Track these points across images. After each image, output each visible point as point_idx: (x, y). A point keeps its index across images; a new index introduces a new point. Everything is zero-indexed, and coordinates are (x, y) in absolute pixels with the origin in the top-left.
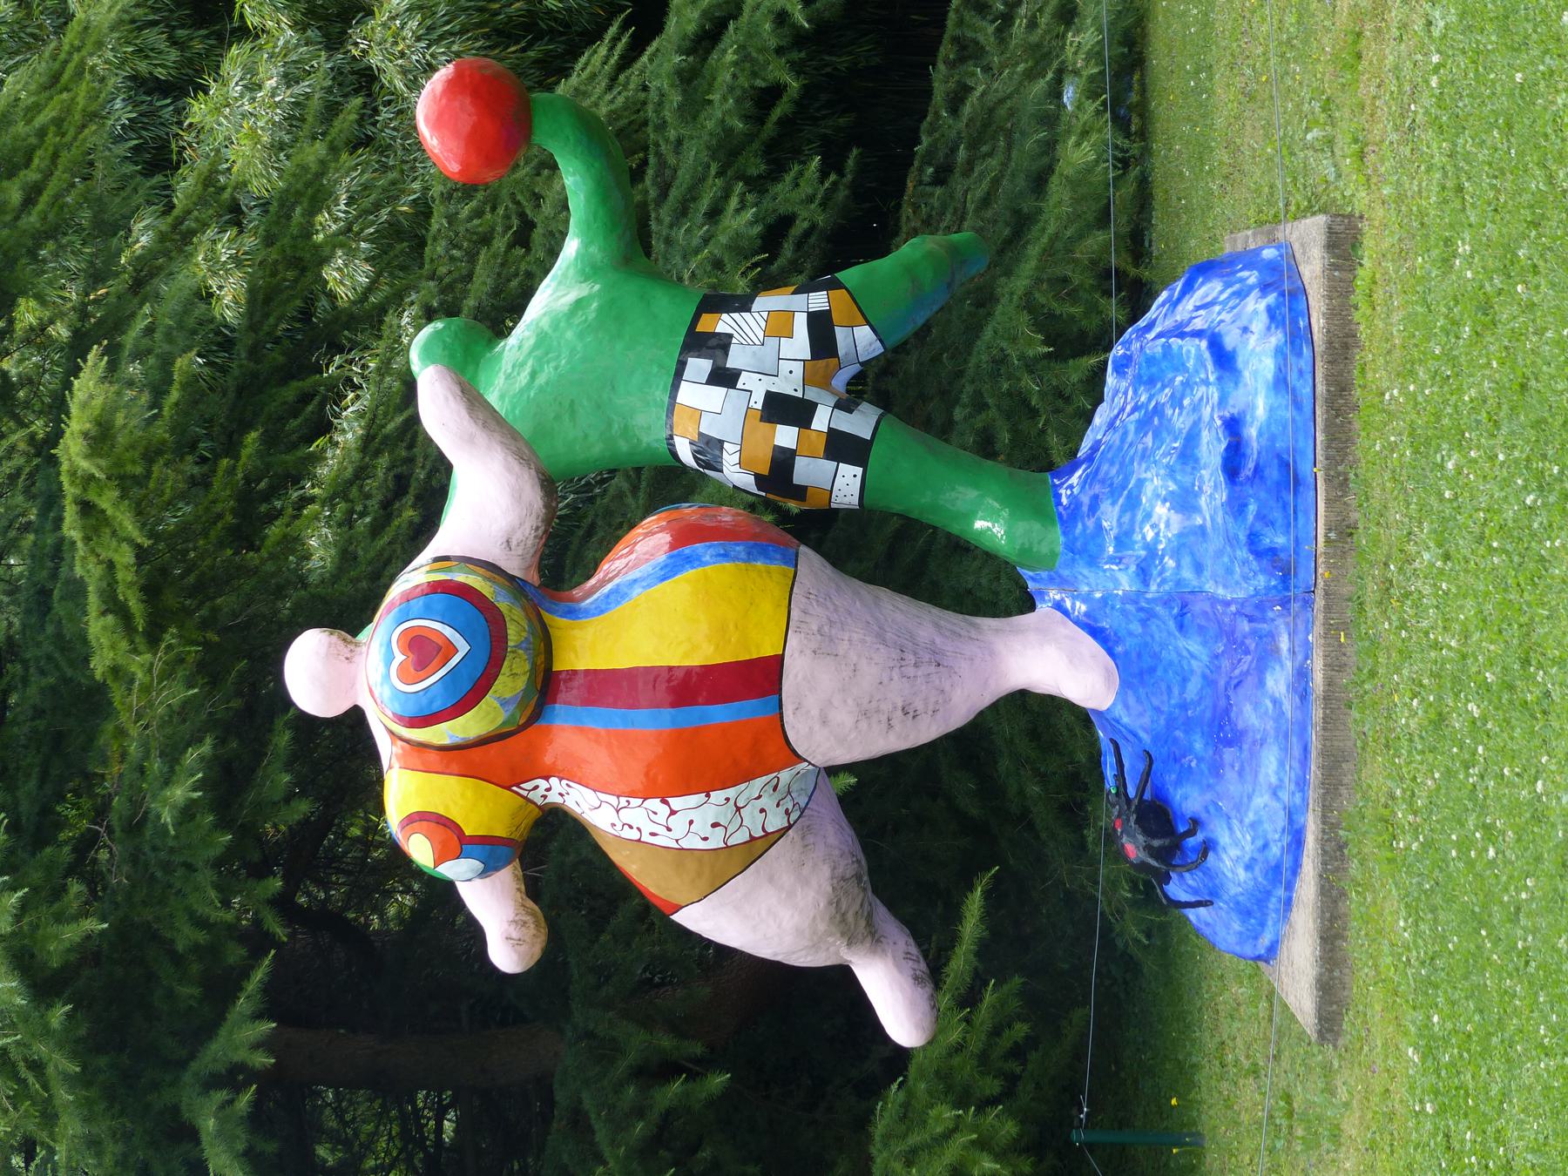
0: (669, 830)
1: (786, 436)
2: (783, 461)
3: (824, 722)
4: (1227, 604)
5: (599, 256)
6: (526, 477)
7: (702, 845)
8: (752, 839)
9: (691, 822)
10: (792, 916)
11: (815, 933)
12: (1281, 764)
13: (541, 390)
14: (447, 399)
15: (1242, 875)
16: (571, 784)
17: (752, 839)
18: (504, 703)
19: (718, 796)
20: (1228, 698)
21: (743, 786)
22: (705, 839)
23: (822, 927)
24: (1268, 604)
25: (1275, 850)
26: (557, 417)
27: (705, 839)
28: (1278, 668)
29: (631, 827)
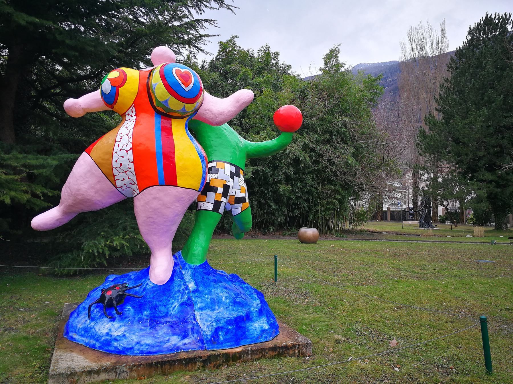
0: (120, 150)
1: (220, 190)
2: (214, 190)
3: (155, 198)
4: (195, 319)
5: (249, 148)
6: (226, 117)
7: (114, 160)
8: (114, 176)
9: (123, 157)
10: (85, 188)
11: (77, 195)
12: (148, 345)
13: (223, 131)
14: (249, 96)
15: (105, 331)
16: (134, 122)
17: (114, 176)
18: (166, 101)
19: (132, 165)
20: (166, 322)
21: (134, 173)
22: (116, 161)
23: (79, 197)
24: (199, 335)
25: (116, 344)
26: (217, 134)
27: (116, 161)
28: (179, 340)
29: (121, 139)
